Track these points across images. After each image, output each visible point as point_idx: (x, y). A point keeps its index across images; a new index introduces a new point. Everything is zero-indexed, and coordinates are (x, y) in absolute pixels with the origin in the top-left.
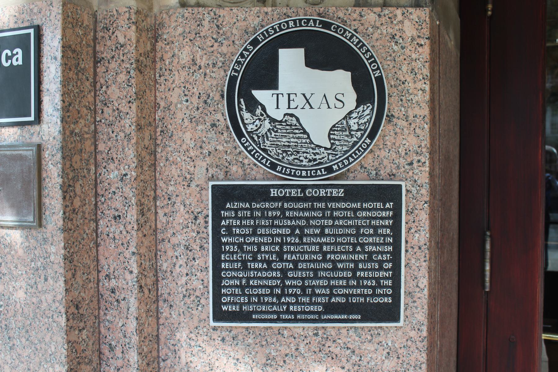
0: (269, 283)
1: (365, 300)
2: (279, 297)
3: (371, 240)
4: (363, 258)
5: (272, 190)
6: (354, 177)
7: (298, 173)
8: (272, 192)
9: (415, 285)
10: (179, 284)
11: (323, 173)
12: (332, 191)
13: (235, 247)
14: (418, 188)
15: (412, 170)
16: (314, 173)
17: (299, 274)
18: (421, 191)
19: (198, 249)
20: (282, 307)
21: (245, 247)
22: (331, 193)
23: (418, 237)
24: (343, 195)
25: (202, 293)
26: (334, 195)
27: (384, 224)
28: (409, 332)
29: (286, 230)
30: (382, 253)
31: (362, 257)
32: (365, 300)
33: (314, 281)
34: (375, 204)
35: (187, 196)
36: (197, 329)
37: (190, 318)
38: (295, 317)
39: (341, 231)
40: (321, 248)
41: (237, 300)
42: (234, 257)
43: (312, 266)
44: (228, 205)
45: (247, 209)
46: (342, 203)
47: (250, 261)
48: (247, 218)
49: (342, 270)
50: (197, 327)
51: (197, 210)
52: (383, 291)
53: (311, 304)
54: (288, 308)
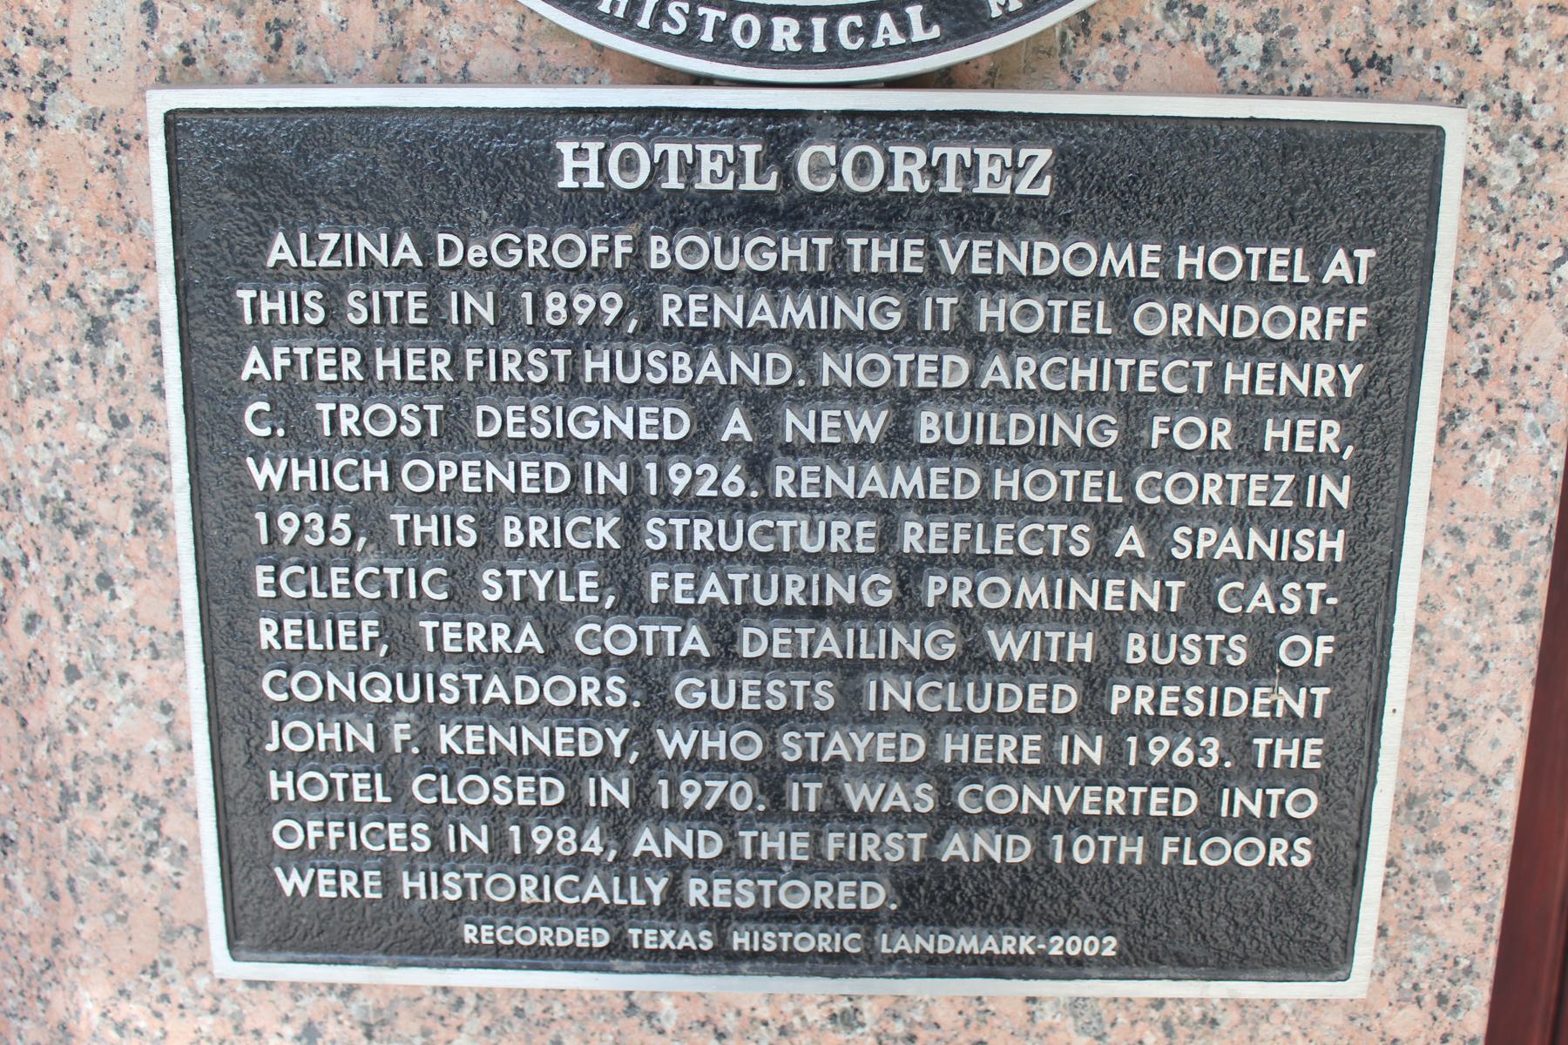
0: (560, 742)
1: (1153, 849)
2: (619, 824)
3: (1212, 492)
4: (1154, 604)
5: (566, 148)
6: (1120, 73)
7: (747, 30)
8: (569, 164)
9: (1448, 756)
10: (35, 724)
11: (918, 34)
12: (975, 158)
13: (339, 520)
14: (1532, 156)
15: (1507, 33)
16: (853, 31)
17: (746, 693)
18: (1548, 179)
19: (128, 524)
20: (642, 885)
21: (400, 519)
22: (969, 172)
23: (1499, 471)
24: (1044, 189)
25: (169, 782)
26: (983, 187)
27: (1303, 388)
28: (1386, 1011)
29: (660, 417)
30: (1279, 571)
31: (1145, 593)
32: (1153, 849)
33: (837, 738)
34: (1256, 252)
35: (35, 185)
36: (155, 975)
37: (111, 918)
38: (722, 939)
39: (1022, 425)
40: (888, 534)
41: (362, 837)
42: (335, 582)
43: (828, 643)
44: (279, 251)
45: (401, 275)
46: (1039, 246)
47: (435, 610)
48: (403, 334)
49: (1020, 671)
50: (155, 965)
51: (100, 281)
52: (1267, 800)
53: (814, 867)
54: (674, 892)
